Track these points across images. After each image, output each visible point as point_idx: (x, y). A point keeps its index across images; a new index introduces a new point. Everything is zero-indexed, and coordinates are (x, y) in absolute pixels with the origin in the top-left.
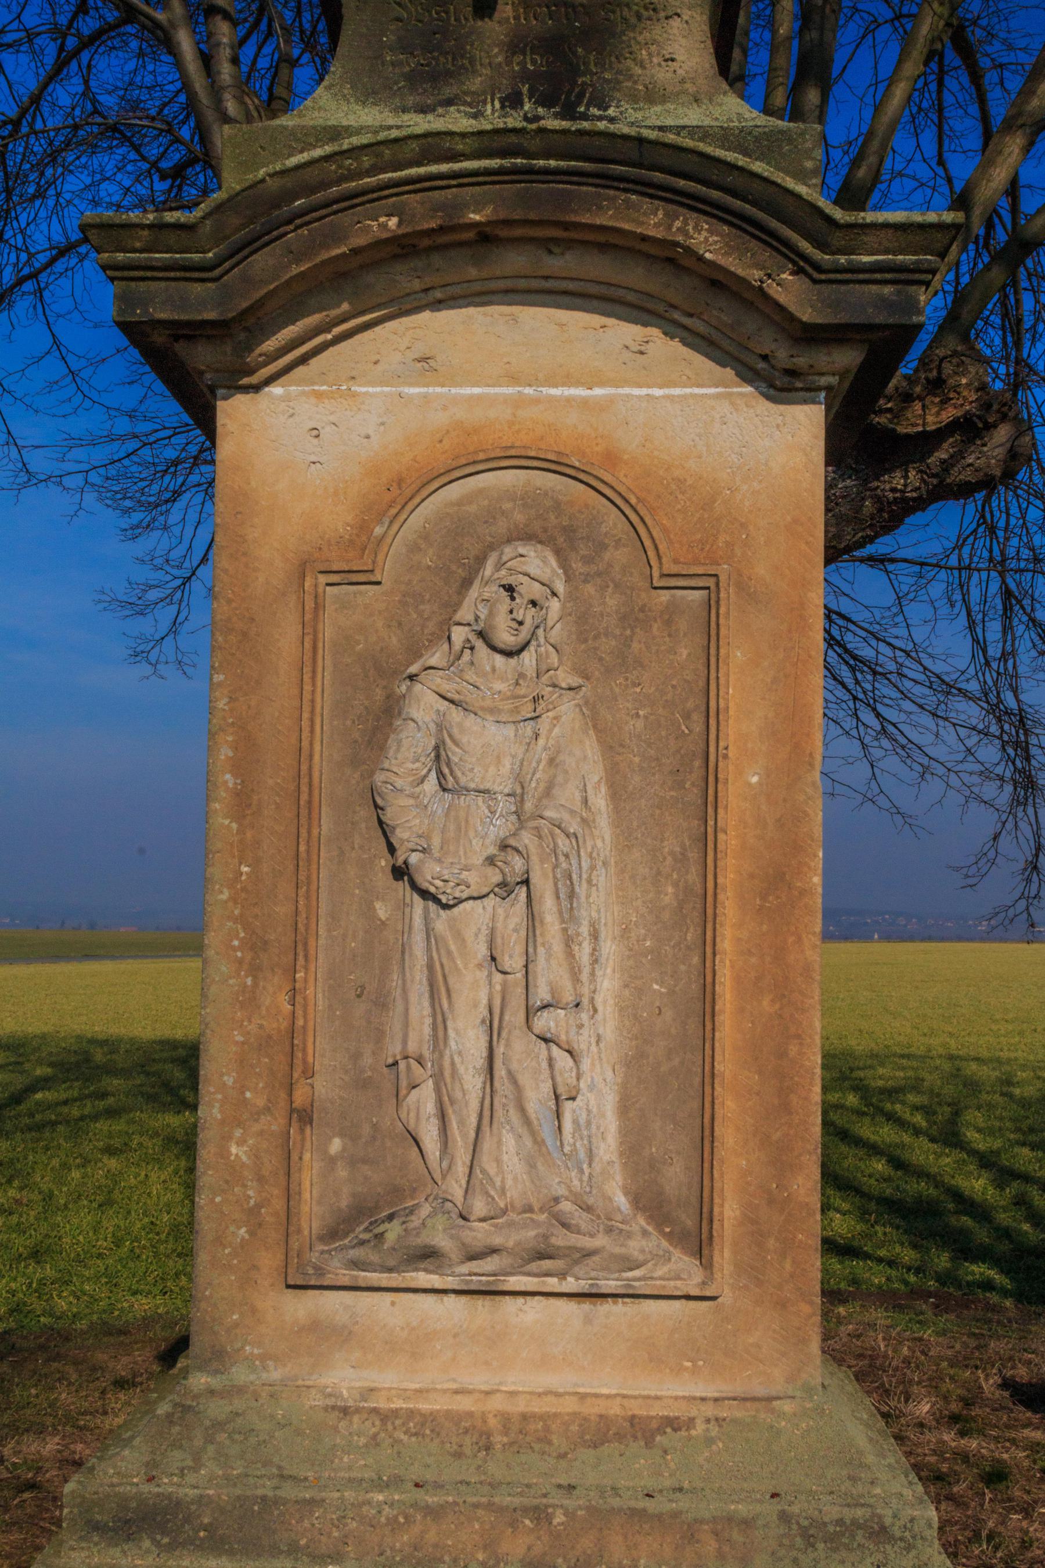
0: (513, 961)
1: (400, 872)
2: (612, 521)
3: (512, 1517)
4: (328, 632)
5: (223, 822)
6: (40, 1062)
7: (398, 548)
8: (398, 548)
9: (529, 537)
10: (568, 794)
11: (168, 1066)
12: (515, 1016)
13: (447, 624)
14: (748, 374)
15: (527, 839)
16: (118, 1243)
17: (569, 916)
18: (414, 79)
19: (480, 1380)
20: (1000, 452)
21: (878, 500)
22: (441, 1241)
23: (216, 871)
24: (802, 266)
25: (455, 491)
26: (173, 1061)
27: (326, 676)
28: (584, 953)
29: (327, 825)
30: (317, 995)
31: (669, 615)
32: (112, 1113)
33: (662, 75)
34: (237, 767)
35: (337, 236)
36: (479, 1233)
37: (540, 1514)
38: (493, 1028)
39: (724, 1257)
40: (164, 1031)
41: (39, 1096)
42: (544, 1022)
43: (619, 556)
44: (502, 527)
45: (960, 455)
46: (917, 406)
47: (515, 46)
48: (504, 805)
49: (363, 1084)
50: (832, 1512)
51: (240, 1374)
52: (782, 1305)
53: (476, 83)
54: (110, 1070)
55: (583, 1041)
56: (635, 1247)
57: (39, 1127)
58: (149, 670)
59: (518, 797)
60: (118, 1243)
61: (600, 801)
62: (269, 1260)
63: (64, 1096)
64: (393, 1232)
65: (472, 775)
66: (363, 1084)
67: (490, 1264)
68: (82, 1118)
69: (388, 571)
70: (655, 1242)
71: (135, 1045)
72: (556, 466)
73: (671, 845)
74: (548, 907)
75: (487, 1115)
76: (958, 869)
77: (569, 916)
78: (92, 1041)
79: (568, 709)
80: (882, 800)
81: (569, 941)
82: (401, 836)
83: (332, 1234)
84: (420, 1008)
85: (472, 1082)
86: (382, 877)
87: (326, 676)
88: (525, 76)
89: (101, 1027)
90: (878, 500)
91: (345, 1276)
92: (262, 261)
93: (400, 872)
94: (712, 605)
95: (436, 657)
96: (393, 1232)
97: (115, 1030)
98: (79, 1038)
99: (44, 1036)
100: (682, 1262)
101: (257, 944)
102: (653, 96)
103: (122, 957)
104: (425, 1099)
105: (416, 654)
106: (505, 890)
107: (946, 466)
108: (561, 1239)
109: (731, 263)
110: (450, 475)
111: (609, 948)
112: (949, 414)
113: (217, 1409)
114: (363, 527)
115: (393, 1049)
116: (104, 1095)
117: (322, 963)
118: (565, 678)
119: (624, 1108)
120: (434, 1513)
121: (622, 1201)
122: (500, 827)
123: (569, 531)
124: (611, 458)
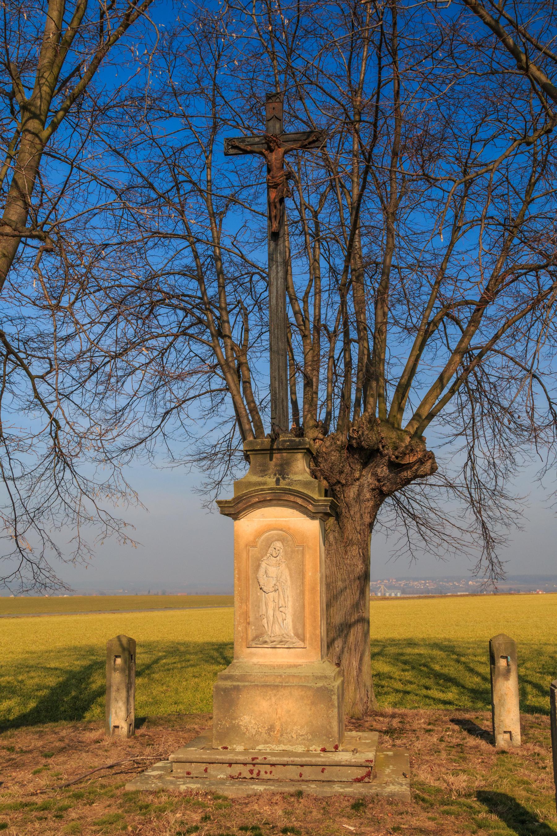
0: (276, 601)
1: (261, 589)
2: (289, 538)
3: (277, 676)
4: (250, 555)
5: (236, 582)
6: (159, 651)
7: (260, 542)
8: (260, 542)
9: (278, 540)
10: (284, 577)
11: (212, 652)
12: (277, 609)
13: (266, 553)
14: (308, 516)
15: (278, 584)
16: (202, 701)
17: (284, 594)
18: (261, 471)
19: (274, 660)
20: (429, 467)
21: (401, 479)
22: (268, 640)
23: (236, 589)
24: (312, 504)
25: (267, 534)
26: (213, 649)
27: (250, 561)
28: (286, 600)
29: (251, 582)
30: (250, 606)
31: (298, 551)
32: (192, 666)
33: (297, 470)
34: (238, 574)
35: (250, 501)
36: (273, 639)
37: (281, 676)
38: (274, 610)
39: (307, 642)
40: (207, 639)
41: (164, 661)
42: (281, 609)
43: (290, 543)
44: (274, 539)
45: (419, 468)
46: (408, 456)
47: (276, 465)
48: (275, 579)
49: (257, 619)
50: (319, 674)
51: (241, 660)
52: (315, 649)
53: (270, 472)
54: (187, 652)
55: (286, 612)
56: (294, 640)
57: (169, 670)
58: (208, 510)
59: (277, 578)
60: (202, 701)
61: (288, 578)
62: (244, 644)
63: (174, 661)
64: (261, 639)
65: (270, 575)
66: (257, 619)
67: (274, 643)
68: (182, 667)
69: (258, 545)
70: (297, 640)
71: (196, 644)
72: (281, 530)
73: (299, 584)
74: (281, 593)
75: (274, 622)
76: (471, 570)
77: (284, 594)
78: (178, 644)
79: (284, 565)
80: (431, 551)
81: (284, 598)
82: (261, 583)
83: (253, 640)
84: (264, 608)
85: (271, 618)
86: (259, 590)
87: (250, 561)
88: (277, 470)
89: (181, 638)
90: (401, 479)
91: (255, 646)
92: (240, 505)
93: (261, 589)
94: (303, 549)
95: (265, 558)
96: (261, 639)
97: (187, 639)
98: (173, 642)
99: (158, 642)
100: (301, 643)
101: (241, 599)
102: (295, 473)
103: (183, 608)
104: (265, 621)
105: (262, 557)
106: (275, 591)
107: (417, 470)
108: (284, 639)
109: (303, 504)
110: (266, 532)
111: (290, 599)
112: (415, 459)
113: (238, 664)
114: (255, 539)
115: (261, 614)
116: (189, 661)
117: (251, 602)
118: (283, 560)
119: (293, 621)
120: (267, 676)
121: (292, 635)
122: (274, 582)
123: (283, 539)
124: (289, 529)
